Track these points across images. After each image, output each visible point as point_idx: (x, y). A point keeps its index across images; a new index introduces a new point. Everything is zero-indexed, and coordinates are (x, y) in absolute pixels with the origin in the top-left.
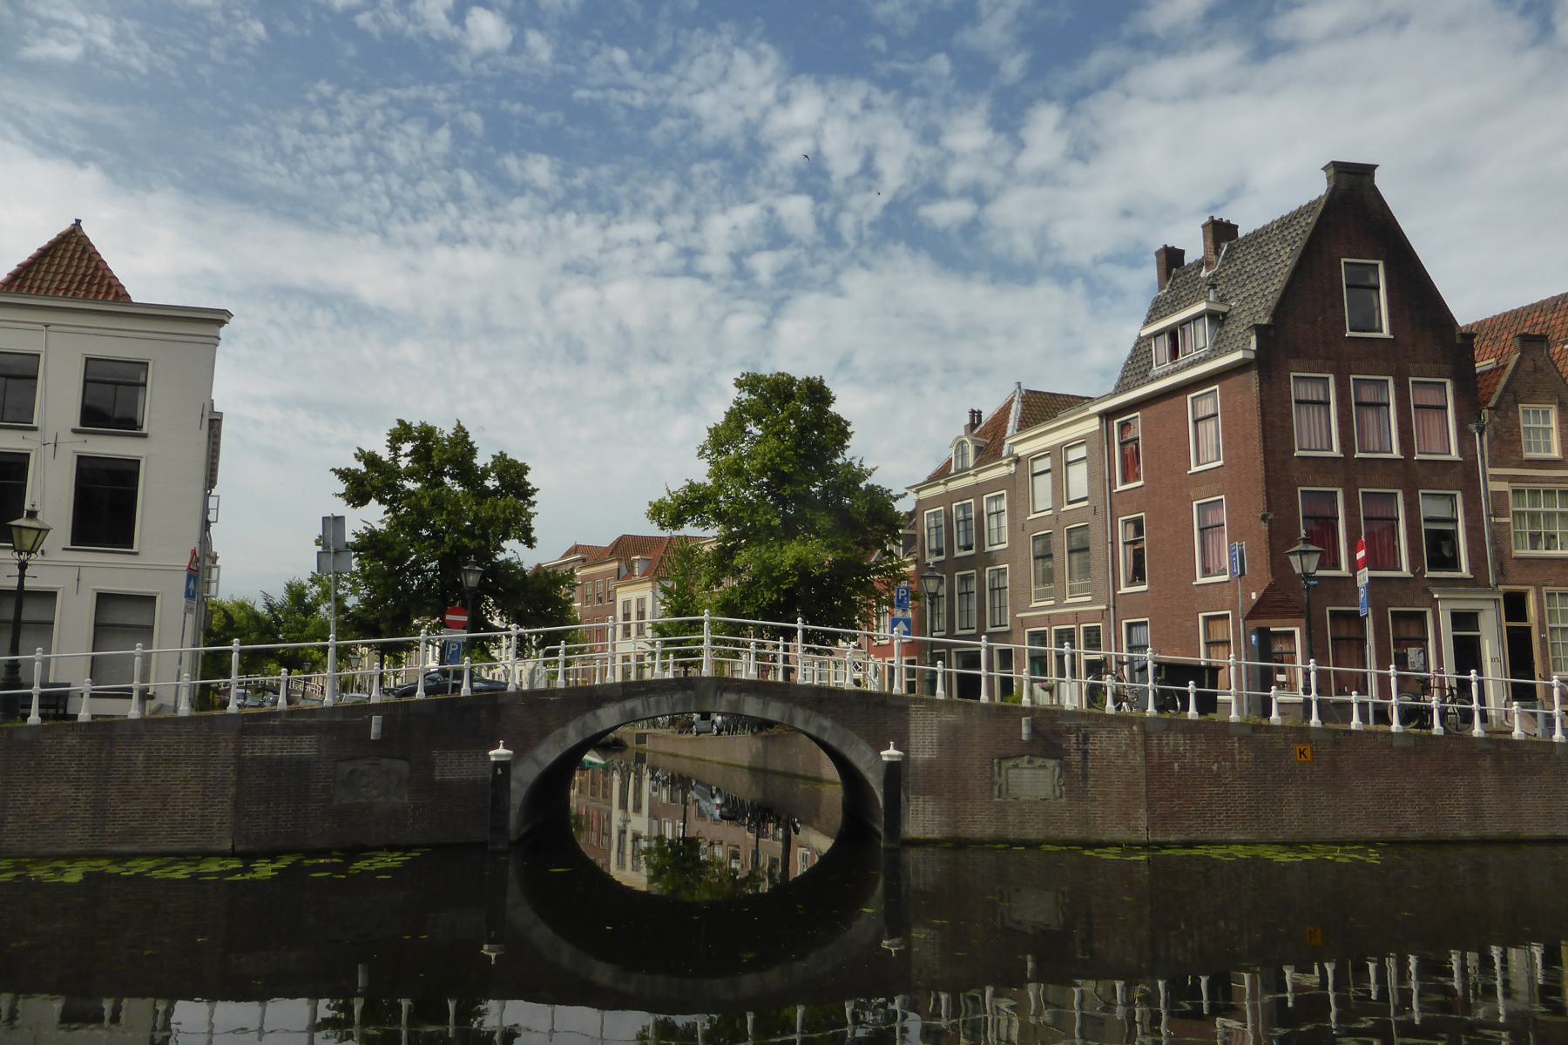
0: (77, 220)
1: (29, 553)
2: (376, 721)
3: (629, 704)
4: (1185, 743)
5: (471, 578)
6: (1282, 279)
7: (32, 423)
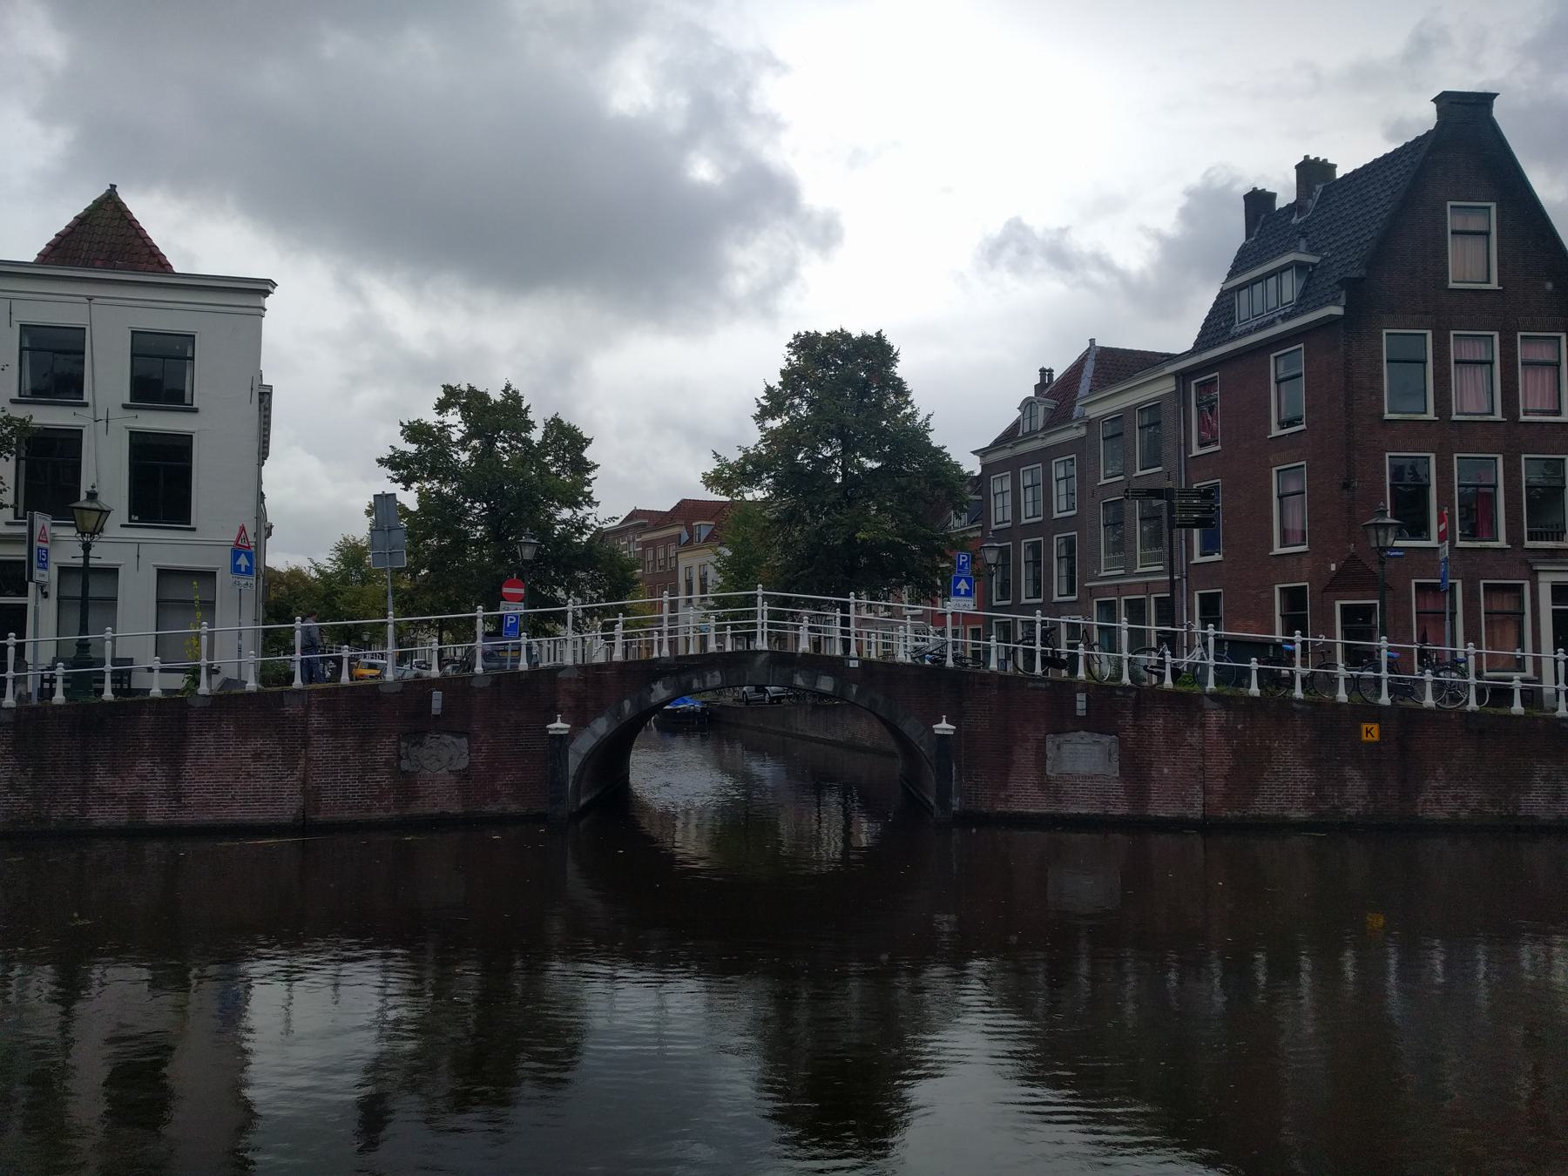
0: (111, 185)
1: (92, 534)
2: (437, 696)
5: (527, 551)
6: (1380, 226)
7: (82, 399)
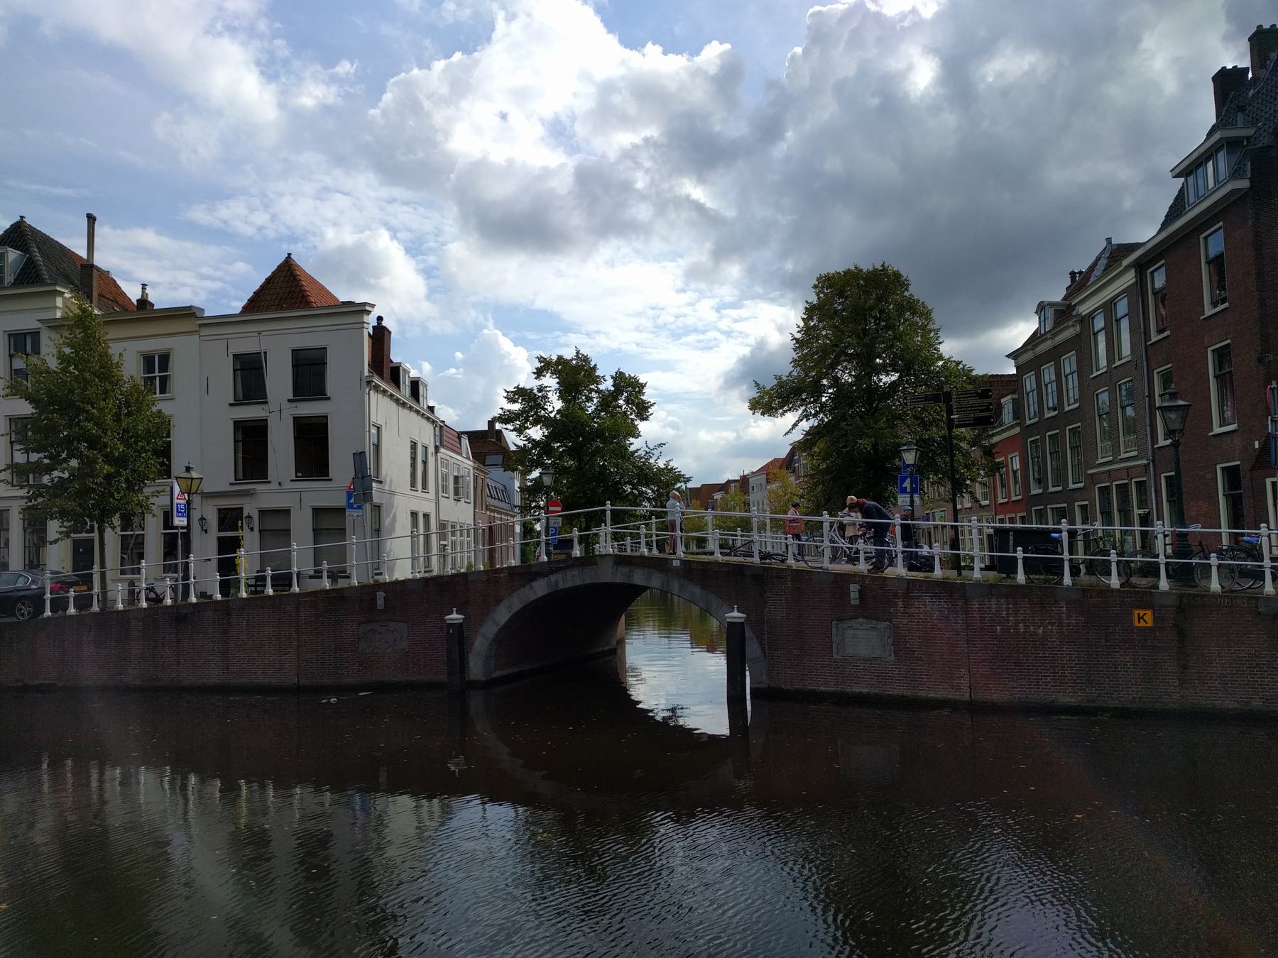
3: (553, 578)
4: (1009, 608)
